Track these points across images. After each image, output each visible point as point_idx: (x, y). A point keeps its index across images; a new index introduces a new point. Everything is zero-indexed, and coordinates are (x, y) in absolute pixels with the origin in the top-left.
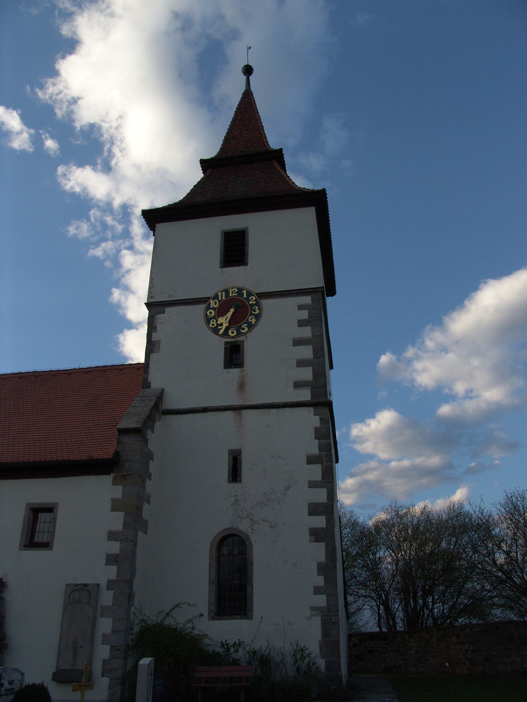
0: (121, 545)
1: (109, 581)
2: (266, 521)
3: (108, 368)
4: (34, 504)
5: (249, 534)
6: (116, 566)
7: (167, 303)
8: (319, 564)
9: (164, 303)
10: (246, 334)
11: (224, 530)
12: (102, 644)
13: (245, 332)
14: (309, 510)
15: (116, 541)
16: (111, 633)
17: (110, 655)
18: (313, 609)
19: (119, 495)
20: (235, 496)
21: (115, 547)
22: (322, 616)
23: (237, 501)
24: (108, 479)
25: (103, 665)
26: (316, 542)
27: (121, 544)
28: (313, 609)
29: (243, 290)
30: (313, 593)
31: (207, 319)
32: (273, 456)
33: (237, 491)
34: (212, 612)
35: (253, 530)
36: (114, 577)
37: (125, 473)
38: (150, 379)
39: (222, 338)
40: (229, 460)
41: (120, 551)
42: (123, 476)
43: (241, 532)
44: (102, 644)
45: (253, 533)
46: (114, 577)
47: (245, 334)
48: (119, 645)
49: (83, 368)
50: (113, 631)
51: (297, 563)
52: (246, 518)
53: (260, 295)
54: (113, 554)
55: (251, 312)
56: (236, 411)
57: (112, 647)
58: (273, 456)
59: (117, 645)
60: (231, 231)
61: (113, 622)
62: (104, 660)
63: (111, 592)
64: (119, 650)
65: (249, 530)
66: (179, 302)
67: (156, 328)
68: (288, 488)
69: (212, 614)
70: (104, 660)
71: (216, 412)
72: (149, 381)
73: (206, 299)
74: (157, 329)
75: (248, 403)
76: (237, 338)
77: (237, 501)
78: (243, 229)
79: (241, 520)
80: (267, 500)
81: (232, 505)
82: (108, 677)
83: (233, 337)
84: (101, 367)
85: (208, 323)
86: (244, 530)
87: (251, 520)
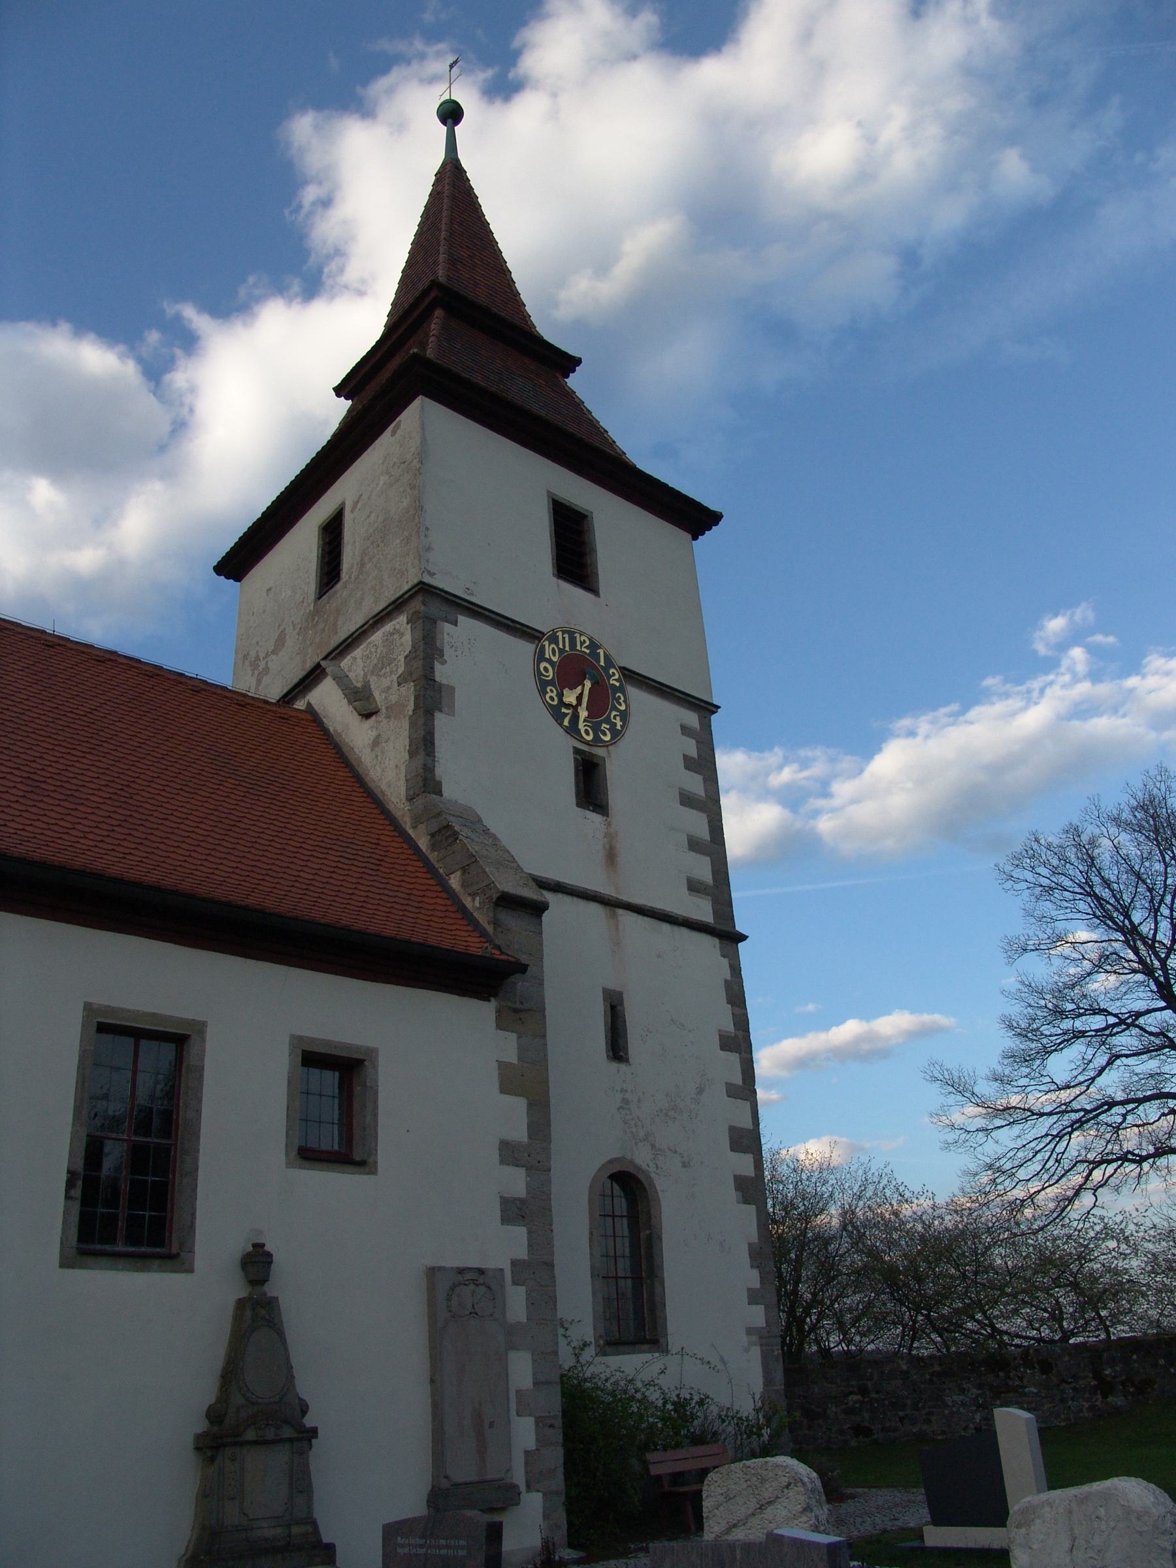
0: (529, 1179)
1: (514, 1263)
2: (676, 1152)
3: (70, 645)
4: (313, 1040)
5: (653, 1175)
6: (524, 1229)
7: (466, 604)
8: (750, 1245)
9: (487, 613)
10: (607, 746)
11: (610, 1162)
12: (518, 1415)
13: (583, 737)
14: (731, 1138)
15: (517, 1166)
16: (532, 1387)
17: (537, 1440)
18: (750, 1331)
19: (512, 1056)
20: (622, 1091)
21: (516, 1182)
22: (761, 1345)
23: (626, 1101)
24: (482, 1012)
25: (526, 1464)
26: (744, 1203)
27: (528, 1175)
28: (750, 1331)
29: (600, 648)
30: (746, 1300)
31: (541, 681)
32: (672, 1020)
33: (624, 1081)
34: (601, 1337)
35: (657, 1167)
36: (522, 1253)
37: (518, 1006)
38: (439, 771)
39: (569, 736)
40: (605, 1012)
41: (528, 1192)
42: (516, 1011)
43: (639, 1168)
44: (518, 1415)
45: (657, 1174)
46: (522, 1253)
47: (606, 745)
48: (552, 1414)
49: (20, 624)
50: (536, 1383)
51: (724, 1241)
52: (645, 1140)
53: (626, 672)
54: (515, 1199)
55: (613, 704)
56: (608, 908)
57: (539, 1421)
58: (672, 1020)
59: (547, 1414)
60: (563, 501)
61: (534, 1361)
62: (527, 1453)
63: (522, 1290)
64: (551, 1426)
65: (652, 1169)
66: (407, 596)
67: (441, 653)
68: (700, 1091)
69: (602, 1342)
70: (527, 1453)
71: (575, 899)
72: (438, 779)
73: (538, 634)
74: (445, 658)
75: (625, 898)
76: (595, 748)
77: (626, 1101)
78: (585, 513)
79: (636, 1144)
80: (673, 1109)
81: (619, 1109)
82: (538, 1491)
83: (587, 743)
84: (125, 657)
85: (543, 692)
86: (644, 1167)
87: (653, 1146)
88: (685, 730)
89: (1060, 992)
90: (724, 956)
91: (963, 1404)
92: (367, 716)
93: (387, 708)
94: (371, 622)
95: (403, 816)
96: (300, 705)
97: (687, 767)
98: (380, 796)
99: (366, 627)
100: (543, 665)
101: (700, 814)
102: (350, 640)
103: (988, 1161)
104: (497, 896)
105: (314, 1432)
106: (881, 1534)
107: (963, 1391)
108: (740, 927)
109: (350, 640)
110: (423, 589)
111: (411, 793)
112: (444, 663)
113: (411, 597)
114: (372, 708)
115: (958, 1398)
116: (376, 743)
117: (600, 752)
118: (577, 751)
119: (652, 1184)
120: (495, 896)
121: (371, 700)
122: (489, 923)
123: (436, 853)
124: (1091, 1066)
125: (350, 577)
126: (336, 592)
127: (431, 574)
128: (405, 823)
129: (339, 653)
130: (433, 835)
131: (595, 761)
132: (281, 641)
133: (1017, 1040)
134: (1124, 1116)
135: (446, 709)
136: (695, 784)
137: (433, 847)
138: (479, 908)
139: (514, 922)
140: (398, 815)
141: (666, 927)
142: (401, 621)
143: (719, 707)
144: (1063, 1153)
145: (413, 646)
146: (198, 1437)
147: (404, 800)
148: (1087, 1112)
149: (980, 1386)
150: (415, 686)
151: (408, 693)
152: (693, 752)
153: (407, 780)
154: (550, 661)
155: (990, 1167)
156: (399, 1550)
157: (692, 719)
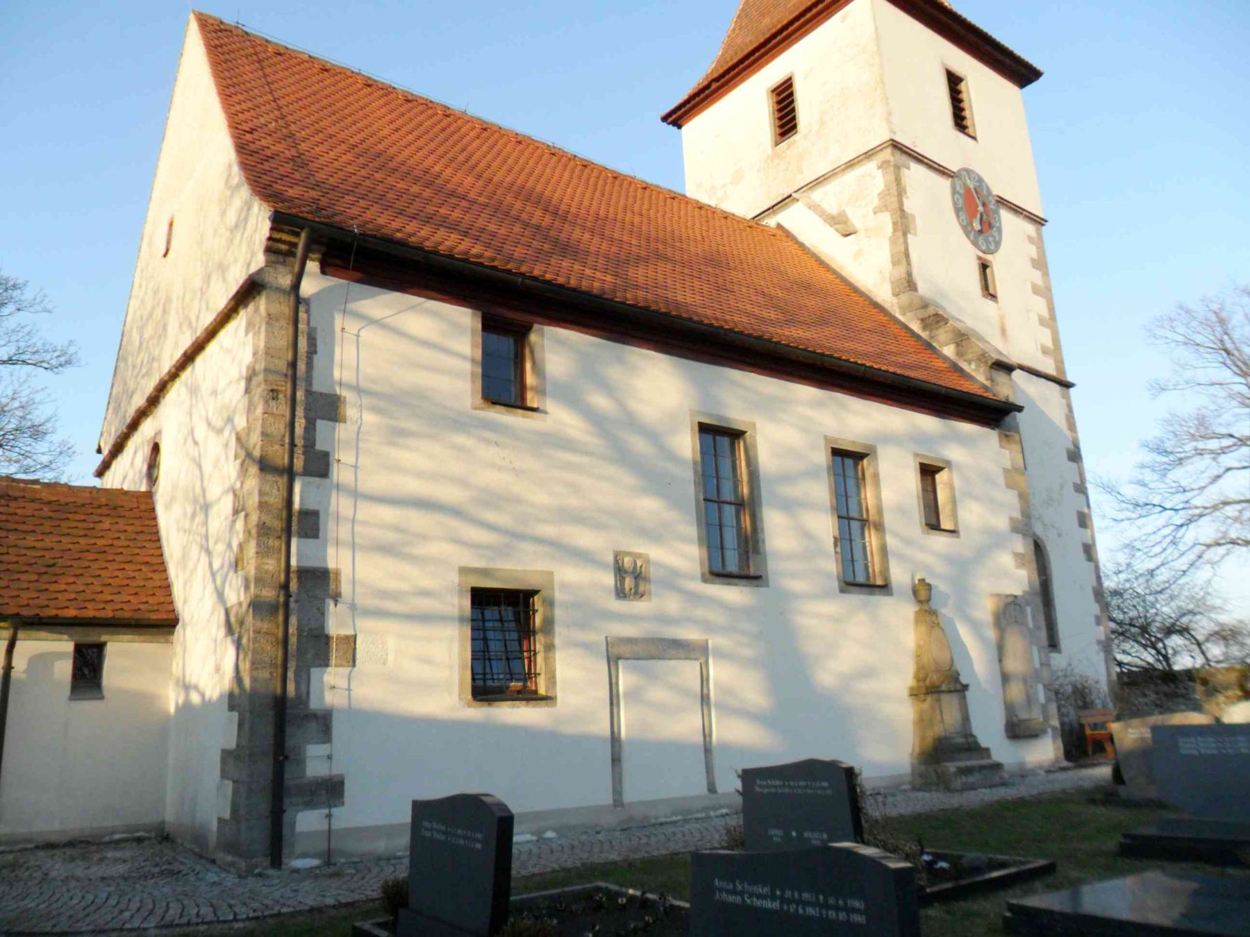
57: (1045, 686)
65: (1044, 538)
88: (1030, 239)
89: (1202, 421)
90: (1063, 398)
91: (1146, 704)
92: (847, 235)
93: (866, 230)
94: (843, 167)
95: (892, 306)
96: (771, 222)
97: (1034, 267)
98: (867, 293)
99: (837, 170)
100: (957, 196)
101: (1041, 298)
102: (822, 179)
103: (1127, 542)
104: (993, 361)
105: (966, 687)
106: (365, 901)
107: (1145, 695)
108: (1070, 378)
109: (822, 179)
110: (896, 146)
111: (897, 290)
112: (907, 198)
113: (881, 150)
114: (851, 230)
115: (1142, 700)
116: (858, 254)
117: (989, 257)
118: (979, 258)
119: (1045, 547)
120: (990, 363)
121: (849, 223)
122: (987, 380)
123: (927, 333)
124: (1205, 475)
125: (810, 131)
126: (794, 142)
127: (895, 133)
128: (895, 311)
129: (811, 188)
130: (923, 320)
131: (988, 264)
132: (738, 177)
133: (1154, 455)
134: (1240, 512)
135: (912, 231)
136: (1036, 276)
137: (925, 328)
138: (976, 370)
139: (1001, 377)
140: (887, 306)
141: (1034, 377)
142: (871, 166)
143: (1046, 221)
144: (1181, 538)
145: (886, 186)
146: (912, 689)
147: (891, 296)
148: (1206, 508)
149: (1157, 693)
150: (892, 215)
151: (886, 220)
152: (1035, 256)
153: (892, 283)
154: (958, 193)
155: (1126, 546)
156: (757, 789)
157: (1030, 228)
